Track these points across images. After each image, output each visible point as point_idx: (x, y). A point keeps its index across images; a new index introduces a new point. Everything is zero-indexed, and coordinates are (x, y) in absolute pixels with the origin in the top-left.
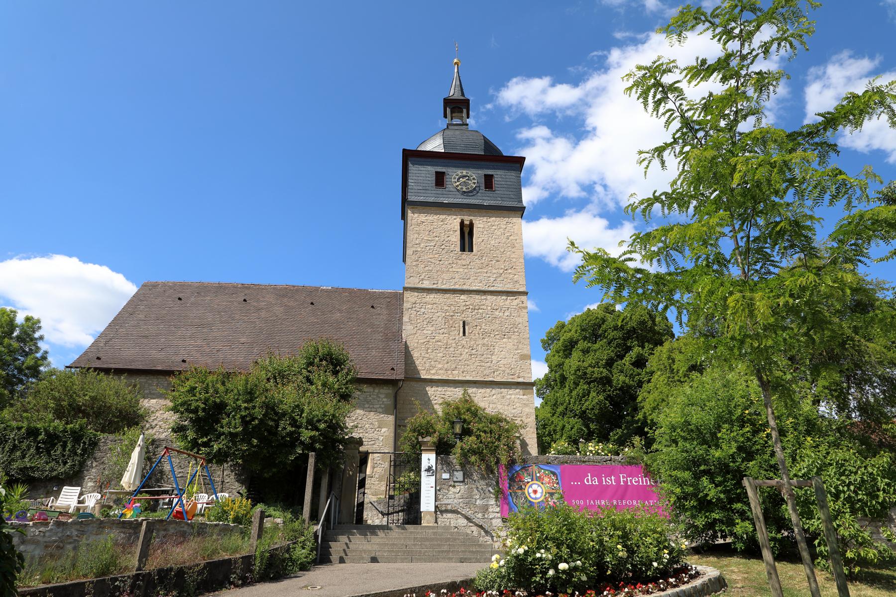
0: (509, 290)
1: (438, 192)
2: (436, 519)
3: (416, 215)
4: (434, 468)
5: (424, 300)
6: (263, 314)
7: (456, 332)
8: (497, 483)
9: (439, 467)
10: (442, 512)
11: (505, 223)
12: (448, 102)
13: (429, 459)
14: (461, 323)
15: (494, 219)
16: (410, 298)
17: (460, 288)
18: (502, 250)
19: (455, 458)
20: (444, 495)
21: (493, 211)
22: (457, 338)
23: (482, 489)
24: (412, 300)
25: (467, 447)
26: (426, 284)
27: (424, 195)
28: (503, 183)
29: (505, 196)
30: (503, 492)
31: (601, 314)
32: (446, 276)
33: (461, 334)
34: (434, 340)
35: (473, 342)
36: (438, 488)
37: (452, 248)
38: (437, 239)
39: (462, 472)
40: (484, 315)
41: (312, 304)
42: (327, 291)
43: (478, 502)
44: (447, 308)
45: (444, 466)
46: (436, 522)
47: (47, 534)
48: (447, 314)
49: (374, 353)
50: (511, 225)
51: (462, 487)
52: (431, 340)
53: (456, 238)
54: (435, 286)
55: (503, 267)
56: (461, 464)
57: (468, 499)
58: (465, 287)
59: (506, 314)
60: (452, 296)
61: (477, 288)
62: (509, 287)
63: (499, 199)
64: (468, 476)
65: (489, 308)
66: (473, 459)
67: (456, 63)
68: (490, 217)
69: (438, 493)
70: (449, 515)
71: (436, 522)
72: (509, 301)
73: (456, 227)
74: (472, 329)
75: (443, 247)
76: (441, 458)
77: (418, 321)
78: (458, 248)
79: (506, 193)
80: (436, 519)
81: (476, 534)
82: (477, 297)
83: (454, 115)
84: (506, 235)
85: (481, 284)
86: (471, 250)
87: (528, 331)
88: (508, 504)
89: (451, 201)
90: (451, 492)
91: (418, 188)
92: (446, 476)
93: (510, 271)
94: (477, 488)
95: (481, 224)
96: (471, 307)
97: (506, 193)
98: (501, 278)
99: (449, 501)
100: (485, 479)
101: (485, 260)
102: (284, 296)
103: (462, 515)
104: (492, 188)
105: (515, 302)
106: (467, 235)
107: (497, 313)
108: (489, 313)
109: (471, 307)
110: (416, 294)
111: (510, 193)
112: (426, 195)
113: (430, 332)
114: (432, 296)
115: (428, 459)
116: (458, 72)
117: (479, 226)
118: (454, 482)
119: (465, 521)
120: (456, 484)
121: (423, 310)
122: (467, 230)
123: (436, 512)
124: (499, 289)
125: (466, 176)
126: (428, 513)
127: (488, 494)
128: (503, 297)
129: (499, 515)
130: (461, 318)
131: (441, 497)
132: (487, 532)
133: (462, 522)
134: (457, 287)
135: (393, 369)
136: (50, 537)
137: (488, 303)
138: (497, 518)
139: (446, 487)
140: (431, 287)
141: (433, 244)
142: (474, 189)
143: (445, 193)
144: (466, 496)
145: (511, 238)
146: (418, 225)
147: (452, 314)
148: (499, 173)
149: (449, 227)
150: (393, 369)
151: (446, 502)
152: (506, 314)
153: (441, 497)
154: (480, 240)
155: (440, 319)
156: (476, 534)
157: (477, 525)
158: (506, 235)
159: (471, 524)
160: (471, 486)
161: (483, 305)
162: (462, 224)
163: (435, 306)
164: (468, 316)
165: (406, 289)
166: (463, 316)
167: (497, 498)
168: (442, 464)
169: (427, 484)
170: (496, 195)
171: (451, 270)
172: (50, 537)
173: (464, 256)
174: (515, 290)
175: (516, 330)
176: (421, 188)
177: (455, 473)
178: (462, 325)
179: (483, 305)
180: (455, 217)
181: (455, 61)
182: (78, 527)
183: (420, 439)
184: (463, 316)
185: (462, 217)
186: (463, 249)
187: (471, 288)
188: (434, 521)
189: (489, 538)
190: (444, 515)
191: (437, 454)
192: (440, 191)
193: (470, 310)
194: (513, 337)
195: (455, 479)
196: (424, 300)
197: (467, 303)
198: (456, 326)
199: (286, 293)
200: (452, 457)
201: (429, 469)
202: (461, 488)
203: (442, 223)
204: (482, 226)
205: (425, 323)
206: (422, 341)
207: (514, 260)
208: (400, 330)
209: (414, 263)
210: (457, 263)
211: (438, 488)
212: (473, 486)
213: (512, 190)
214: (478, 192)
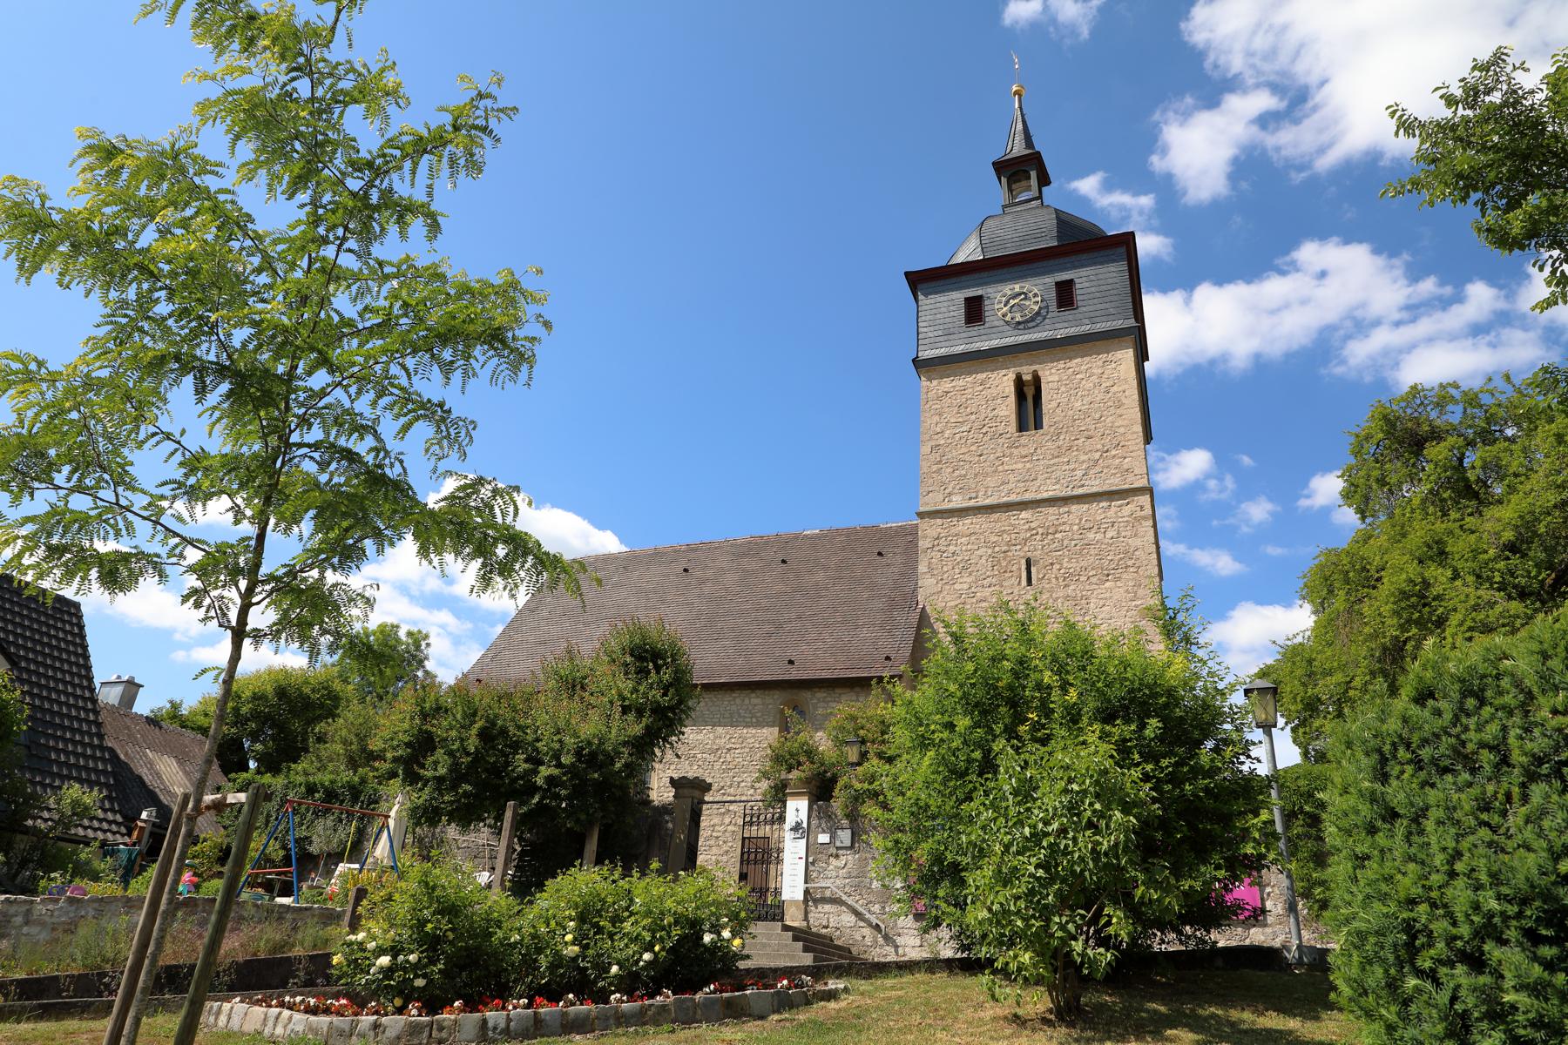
0: (1114, 488)
1: (970, 334)
2: (806, 913)
3: (935, 382)
4: (805, 825)
5: (954, 531)
6: (707, 589)
7: (1014, 581)
9: (814, 822)
10: (816, 902)
11: (1100, 363)
12: (1001, 167)
14: (1023, 562)
15: (1079, 360)
16: (930, 530)
17: (1019, 498)
18: (1097, 416)
19: (838, 805)
21: (1075, 347)
22: (1016, 591)
24: (932, 533)
26: (957, 502)
27: (947, 344)
28: (1093, 289)
29: (1097, 314)
32: (991, 482)
33: (1024, 582)
34: (974, 600)
35: (1048, 595)
36: (811, 859)
37: (1001, 428)
38: (973, 417)
39: (849, 831)
40: (1066, 542)
41: (784, 562)
44: (996, 538)
45: (823, 821)
46: (806, 919)
47: (56, 913)
48: (997, 549)
49: (864, 633)
50: (1113, 365)
51: (850, 857)
52: (969, 601)
53: (1008, 409)
54: (972, 503)
55: (1099, 447)
57: (858, 881)
58: (1028, 496)
59: (1109, 535)
60: (1004, 516)
61: (1051, 493)
62: (1115, 483)
63: (1087, 321)
65: (1076, 528)
67: (1016, 93)
68: (1071, 359)
69: (811, 868)
70: (827, 907)
71: (806, 919)
72: (1113, 509)
73: (1007, 390)
74: (1044, 571)
75: (984, 430)
76: (820, 807)
77: (945, 569)
78: (1013, 427)
79: (1102, 306)
80: (806, 913)
82: (1051, 510)
83: (1014, 186)
84: (1104, 385)
85: (1057, 487)
86: (1038, 425)
89: (995, 343)
91: (936, 334)
92: (824, 838)
93: (1113, 452)
95: (1053, 375)
96: (1040, 531)
97: (1102, 306)
98: (1098, 469)
101: (1064, 440)
102: (744, 555)
103: (849, 906)
104: (1072, 304)
105: (1127, 510)
106: (1029, 399)
107: (1091, 535)
108: (1076, 537)
109: (1040, 531)
110: (939, 521)
111: (1107, 306)
112: (951, 343)
113: (966, 586)
115: (797, 809)
116: (1021, 108)
117: (1050, 379)
118: (838, 848)
120: (841, 852)
121: (952, 548)
122: (1030, 392)
123: (806, 901)
124: (1094, 490)
125: (1020, 294)
126: (795, 902)
128: (1101, 505)
132: (886, 938)
133: (849, 919)
134: (1013, 498)
135: (888, 658)
136: (59, 916)
137: (1073, 518)
140: (965, 505)
141: (965, 428)
142: (1038, 313)
143: (982, 332)
145: (1113, 390)
146: (939, 398)
147: (1004, 548)
148: (1084, 274)
149: (994, 391)
150: (888, 658)
152: (1109, 535)
153: (815, 874)
154: (1054, 404)
155: (983, 560)
156: (868, 941)
157: (870, 924)
158: (1104, 385)
159: (862, 924)
161: (1064, 523)
162: (1019, 383)
164: (1036, 549)
165: (921, 515)
166: (1026, 549)
168: (820, 818)
169: (793, 852)
170: (1081, 316)
171: (1000, 468)
172: (59, 916)
173: (1024, 440)
174: (1126, 486)
175: (1130, 563)
176: (940, 333)
177: (839, 832)
178: (1024, 567)
179: (1064, 523)
180: (1004, 372)
181: (1015, 88)
182: (96, 905)
184: (1026, 549)
185: (1018, 369)
186: (1022, 427)
187: (1039, 497)
188: (801, 916)
189: (890, 949)
192: (975, 330)
193: (1038, 537)
194: (1124, 576)
195: (838, 844)
197: (1033, 525)
198: (1014, 568)
199: (752, 549)
201: (797, 827)
202: (848, 859)
203: (981, 388)
204: (1056, 378)
205: (957, 571)
206: (953, 604)
207: (1122, 430)
209: (935, 468)
210: (1011, 454)
211: (811, 859)
212: (868, 855)
213: (1112, 299)
214: (1045, 318)
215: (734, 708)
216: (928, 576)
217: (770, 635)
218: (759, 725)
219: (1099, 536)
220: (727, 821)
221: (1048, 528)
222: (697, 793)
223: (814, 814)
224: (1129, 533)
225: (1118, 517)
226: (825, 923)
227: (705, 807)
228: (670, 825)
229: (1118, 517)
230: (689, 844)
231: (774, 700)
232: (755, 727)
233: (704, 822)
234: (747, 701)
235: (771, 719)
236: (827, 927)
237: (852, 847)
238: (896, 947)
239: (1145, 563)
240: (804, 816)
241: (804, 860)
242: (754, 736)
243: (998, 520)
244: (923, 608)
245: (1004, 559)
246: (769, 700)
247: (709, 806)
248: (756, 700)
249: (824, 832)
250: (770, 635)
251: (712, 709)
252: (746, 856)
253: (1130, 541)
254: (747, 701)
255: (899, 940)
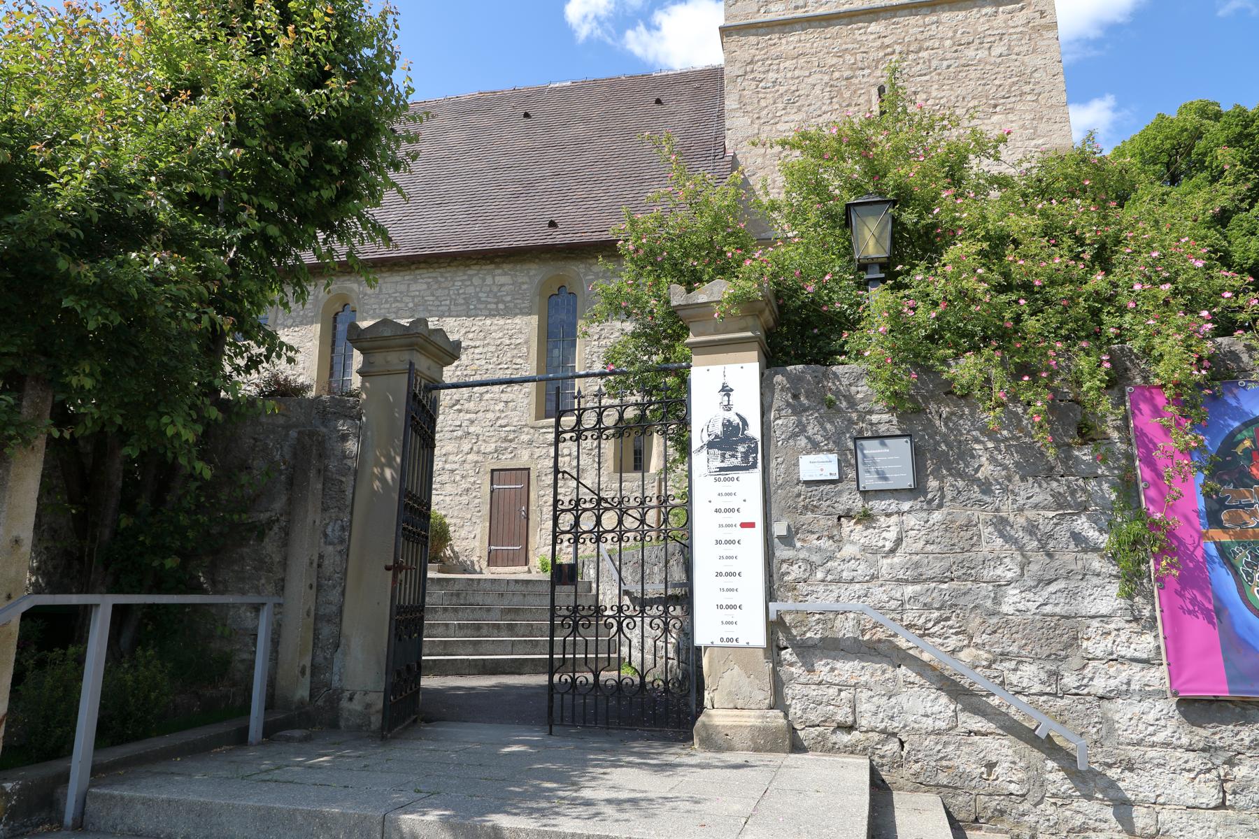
2: (778, 686)
4: (754, 431)
5: (774, 51)
8: (1127, 487)
10: (807, 651)
13: (726, 390)
14: (875, 91)
20: (813, 567)
23: (1031, 529)
25: (925, 316)
30: (1172, 546)
31: (1193, 120)
36: (779, 529)
39: (904, 446)
40: (934, 63)
41: (527, 115)
42: (561, 90)
43: (1012, 600)
44: (835, 60)
46: (778, 702)
48: (836, 75)
51: (911, 521)
54: (799, 13)
56: (897, 402)
59: (997, 50)
60: (845, 30)
64: (943, 461)
65: (948, 43)
66: (965, 369)
69: (782, 552)
70: (847, 669)
71: (778, 702)
72: (1001, 17)
76: (795, 381)
77: (763, 103)
80: (778, 686)
81: (1009, 777)
82: (912, 20)
87: (1062, 87)
88: (1217, 613)
90: (848, 550)
94: (1001, 524)
99: (846, 597)
100: (1050, 474)
102: (472, 112)
103: (923, 668)
107: (970, 53)
108: (948, 55)
109: (898, 48)
110: (753, 39)
114: (793, 38)
118: (866, 494)
119: (943, 705)
120: (877, 505)
121: (772, 76)
123: (773, 649)
126: (732, 650)
127: (1068, 557)
128: (984, 11)
129: (1158, 676)
130: (873, 81)
131: (795, 572)
138: (1146, 694)
139: (825, 522)
144: (936, 568)
147: (848, 73)
151: (822, 599)
152: (997, 50)
153: (795, 572)
155: (817, 90)
159: (977, 723)
160: (962, 516)
161: (931, 38)
163: (802, 61)
167: (1132, 580)
168: (798, 410)
175: (1027, 88)
177: (871, 448)
179: (931, 38)
183: (678, 295)
188: (763, 695)
190: (822, 668)
191: (772, 360)
194: (1019, 106)
195: (870, 481)
196: (774, 51)
197: (887, 41)
198: (862, 100)
200: (844, 370)
205: (780, 106)
208: (719, 136)
211: (779, 529)
212: (977, 514)
215: (471, 290)
216: (739, 114)
217: (516, 196)
218: (509, 312)
219: (982, 54)
220: (466, 447)
221: (909, 43)
222: (423, 364)
223: (779, 400)
224: (1025, 48)
225: (1008, 27)
226: (843, 715)
227: (446, 397)
228: (352, 446)
229: (1008, 27)
230: (405, 493)
231: (530, 277)
232: (503, 316)
233: (445, 421)
234: (489, 280)
235: (527, 304)
236: (850, 728)
237: (917, 490)
238: (1123, 806)
239: (1048, 88)
240: (748, 404)
241: (759, 529)
242: (501, 329)
243: (838, 36)
244: (734, 157)
245: (847, 87)
246: (521, 278)
247: (447, 391)
248: (502, 279)
249: (815, 447)
250: (516, 196)
251: (439, 293)
252: (566, 520)
253: (1026, 59)
254: (489, 280)
255: (1129, 783)
